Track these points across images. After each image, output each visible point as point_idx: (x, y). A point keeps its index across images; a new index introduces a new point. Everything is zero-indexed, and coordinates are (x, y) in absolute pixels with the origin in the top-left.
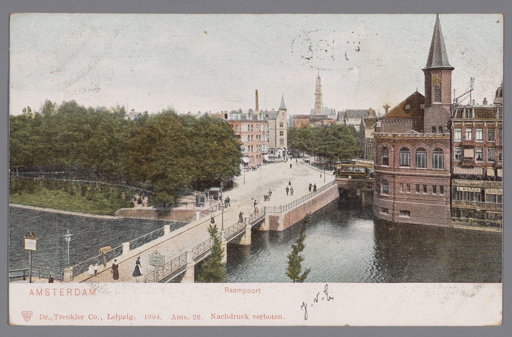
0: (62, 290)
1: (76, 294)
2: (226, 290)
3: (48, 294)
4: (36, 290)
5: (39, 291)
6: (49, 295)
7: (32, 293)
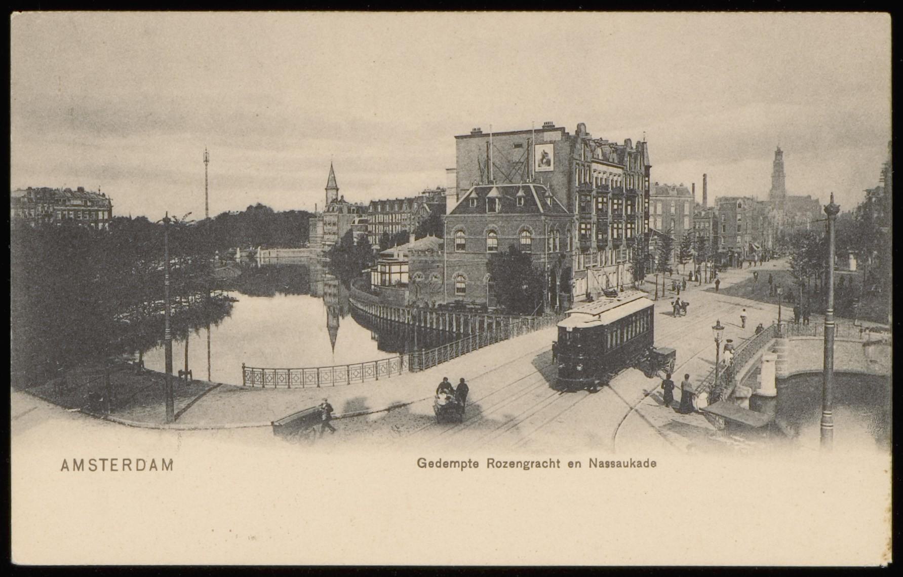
0: (114, 462)
1: (139, 468)
2: (124, 465)
3: (93, 467)
4: (151, 461)
5: (167, 462)
6: (96, 469)
7: (65, 466)
